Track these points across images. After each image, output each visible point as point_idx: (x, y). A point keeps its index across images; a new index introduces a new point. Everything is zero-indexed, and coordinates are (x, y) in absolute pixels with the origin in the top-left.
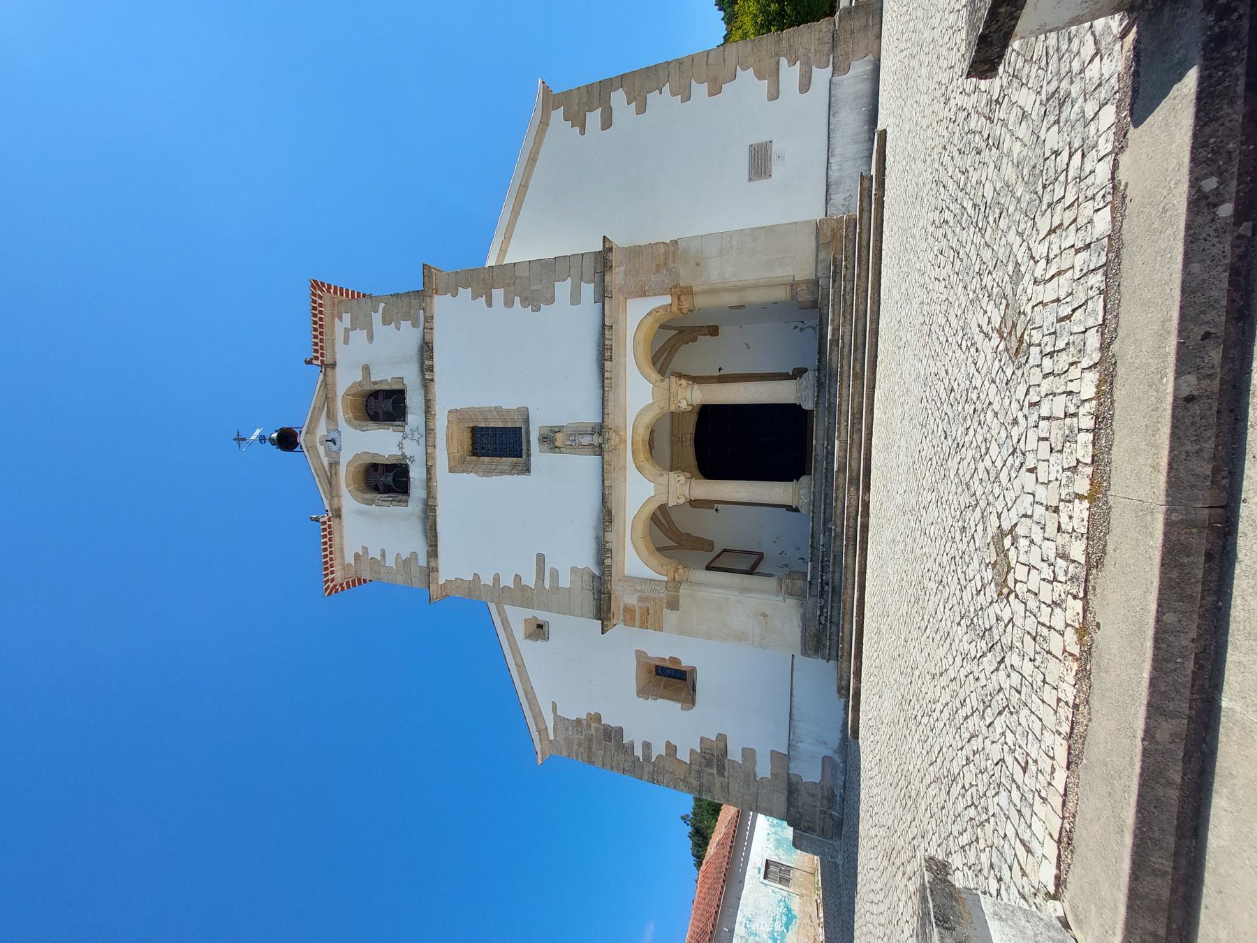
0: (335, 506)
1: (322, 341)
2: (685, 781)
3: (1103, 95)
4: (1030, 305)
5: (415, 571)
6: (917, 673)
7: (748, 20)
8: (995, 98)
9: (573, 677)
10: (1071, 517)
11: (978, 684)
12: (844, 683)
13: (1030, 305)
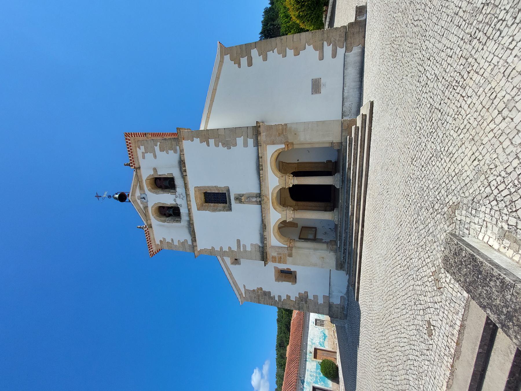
0: (149, 224)
9: (251, 276)
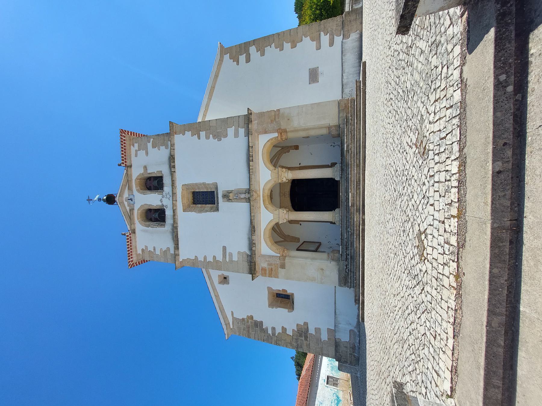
1: (125, 155)
2: (291, 343)
3: (455, 41)
4: (428, 133)
5: (169, 257)
6: (387, 294)
7: (307, 18)
8: (409, 45)
9: (240, 300)
10: (450, 226)
11: (413, 299)
12: (357, 298)
13: (428, 133)
